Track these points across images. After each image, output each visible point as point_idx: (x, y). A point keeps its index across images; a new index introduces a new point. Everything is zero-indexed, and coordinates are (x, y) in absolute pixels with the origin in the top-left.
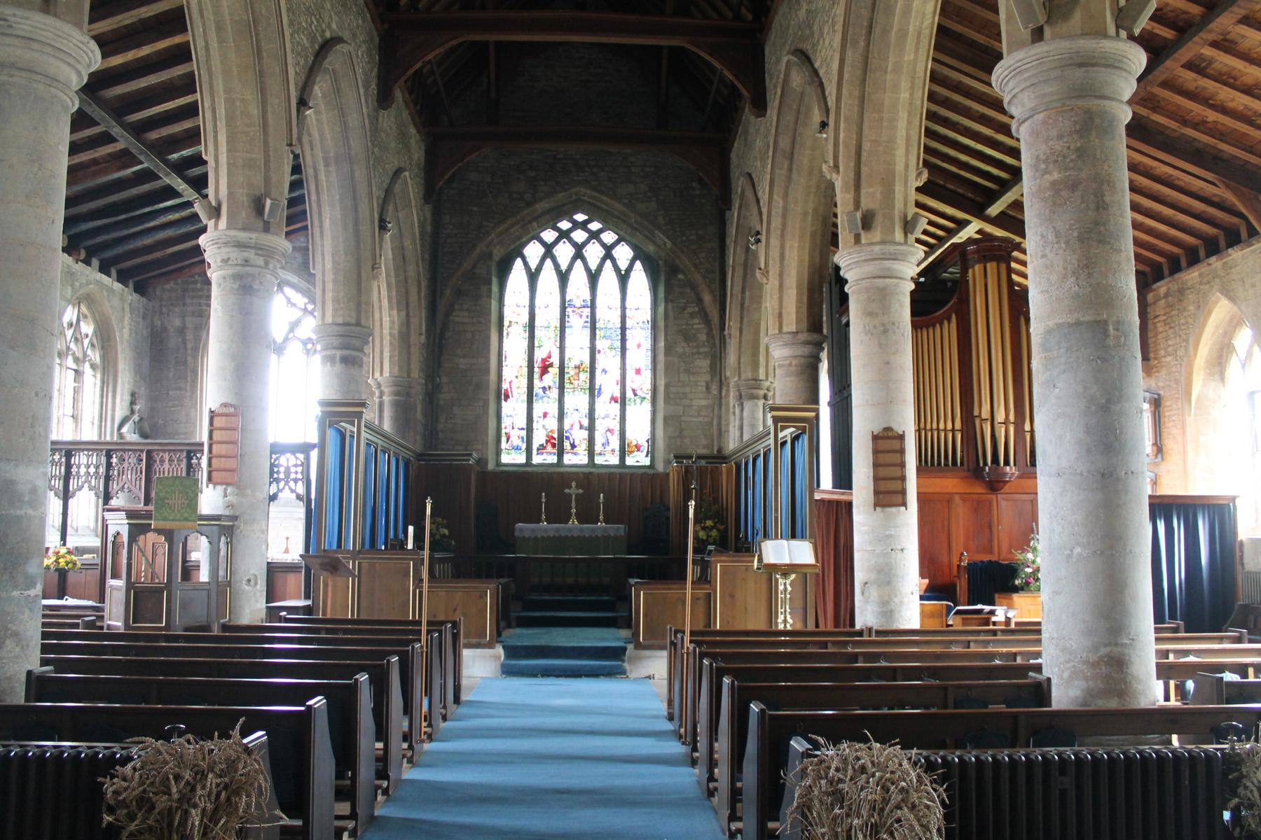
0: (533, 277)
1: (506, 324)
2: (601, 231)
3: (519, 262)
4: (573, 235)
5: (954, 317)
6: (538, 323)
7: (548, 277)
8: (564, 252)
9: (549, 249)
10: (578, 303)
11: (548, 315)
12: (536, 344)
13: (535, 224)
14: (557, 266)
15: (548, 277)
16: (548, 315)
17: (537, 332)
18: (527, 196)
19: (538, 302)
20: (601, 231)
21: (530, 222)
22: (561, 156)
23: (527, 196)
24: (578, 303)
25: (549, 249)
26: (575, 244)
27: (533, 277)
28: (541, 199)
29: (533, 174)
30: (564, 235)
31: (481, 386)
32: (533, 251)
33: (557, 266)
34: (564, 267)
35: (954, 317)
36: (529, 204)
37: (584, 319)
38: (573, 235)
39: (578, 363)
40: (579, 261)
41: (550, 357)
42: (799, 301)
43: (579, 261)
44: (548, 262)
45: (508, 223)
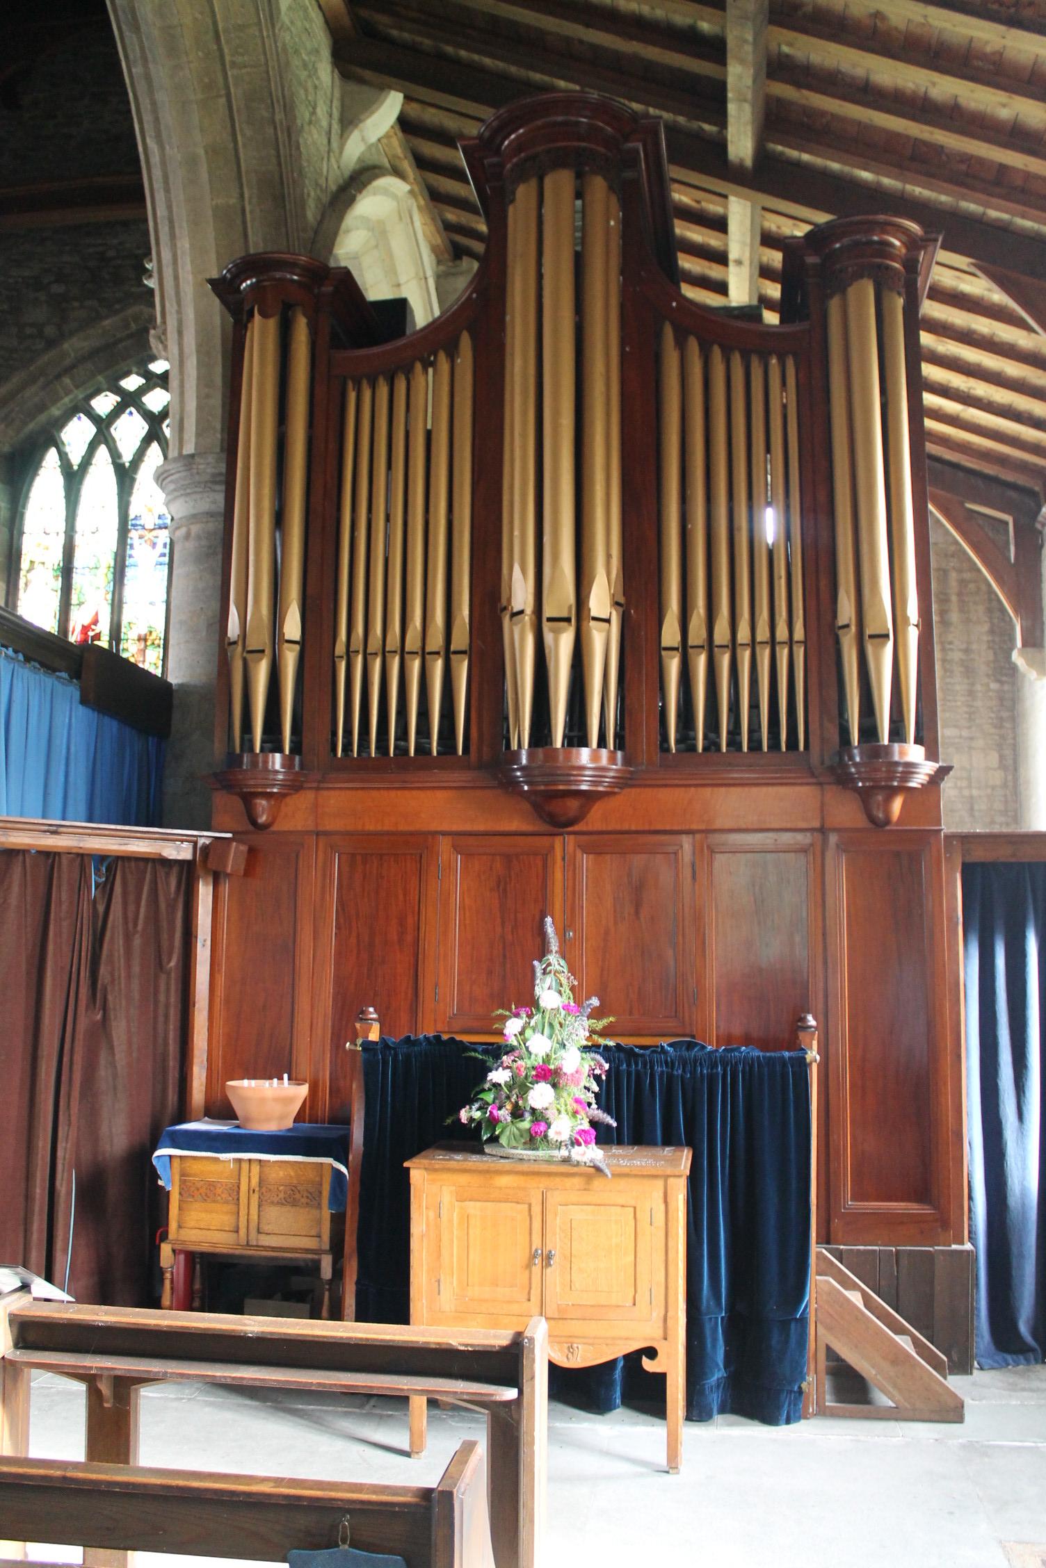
0: (73, 477)
1: (25, 565)
2: (142, 391)
3: (52, 456)
4: (145, 399)
5: (466, 342)
6: (78, 561)
7: (100, 479)
8: (129, 430)
9: (103, 425)
10: (149, 521)
11: (96, 549)
12: (74, 600)
13: (67, 381)
14: (115, 455)
15: (100, 479)
16: (96, 549)
17: (77, 579)
18: (50, 330)
19: (80, 524)
20: (142, 391)
21: (58, 377)
22: (111, 253)
23: (50, 330)
24: (149, 521)
25: (103, 425)
26: (148, 415)
27: (73, 477)
28: (71, 334)
29: (58, 289)
30: (130, 400)
31: (876, 190)
32: (77, 433)
33: (115, 455)
34: (127, 458)
35: (466, 342)
36: (51, 343)
37: (160, 549)
38: (145, 399)
39: (143, 632)
40: (155, 445)
41: (95, 622)
42: (361, 1339)
43: (155, 445)
44: (102, 452)
45: (16, 380)
